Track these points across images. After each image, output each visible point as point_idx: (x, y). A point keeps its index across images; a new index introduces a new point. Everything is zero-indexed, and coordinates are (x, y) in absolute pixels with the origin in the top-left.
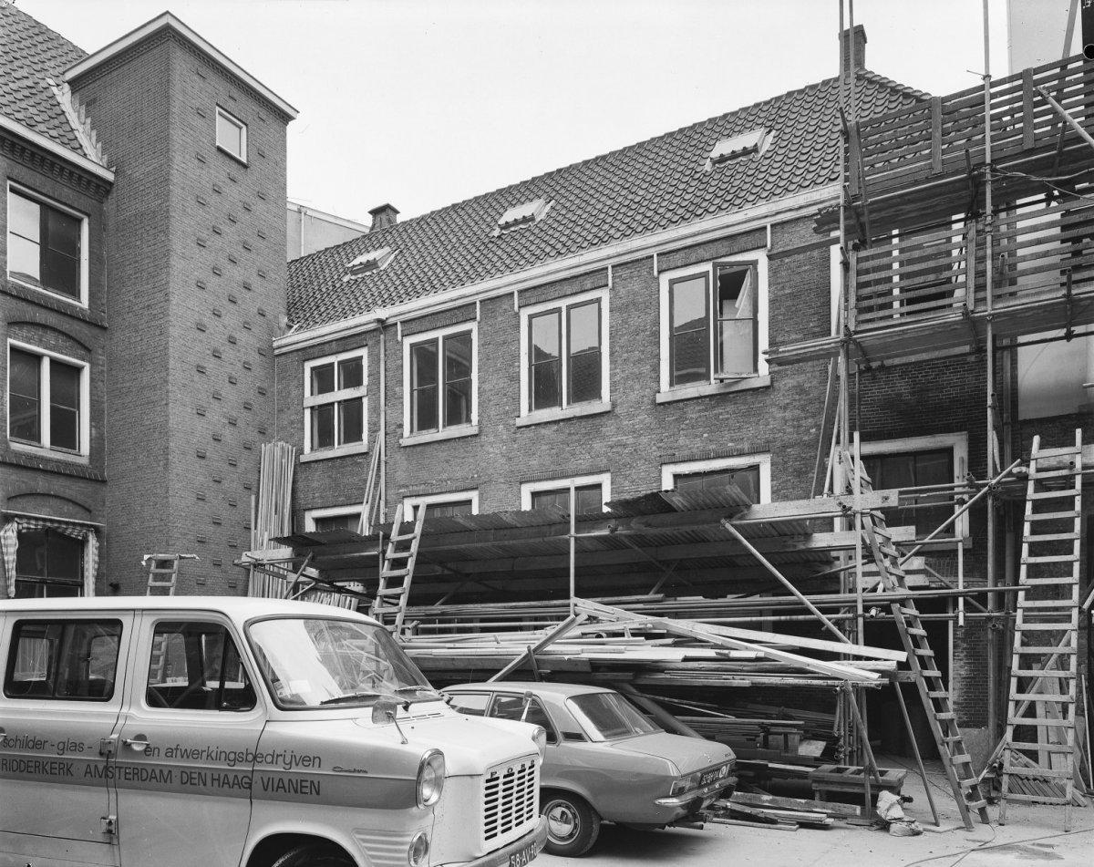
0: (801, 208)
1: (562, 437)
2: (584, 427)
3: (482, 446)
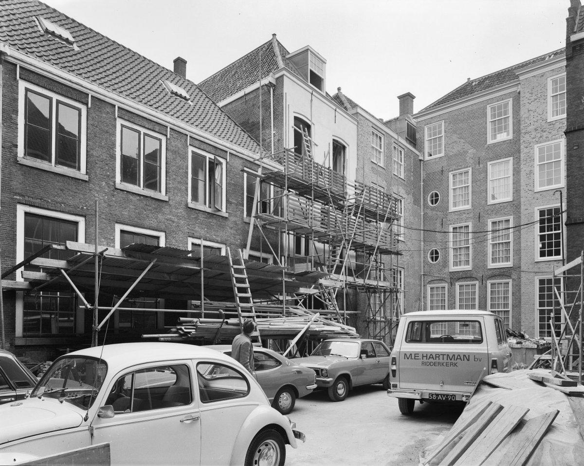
0: (238, 152)
1: (142, 205)
2: (154, 205)
3: (90, 190)
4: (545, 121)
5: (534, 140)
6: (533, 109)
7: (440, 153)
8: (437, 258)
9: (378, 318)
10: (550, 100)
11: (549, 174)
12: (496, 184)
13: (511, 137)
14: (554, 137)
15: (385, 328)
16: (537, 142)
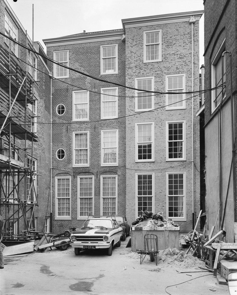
4: (142, 62)
5: (135, 74)
6: (134, 51)
7: (65, 75)
8: (63, 156)
9: (11, 201)
10: (145, 47)
11: (144, 101)
12: (107, 105)
13: (117, 72)
14: (148, 74)
15: (18, 211)
16: (137, 76)
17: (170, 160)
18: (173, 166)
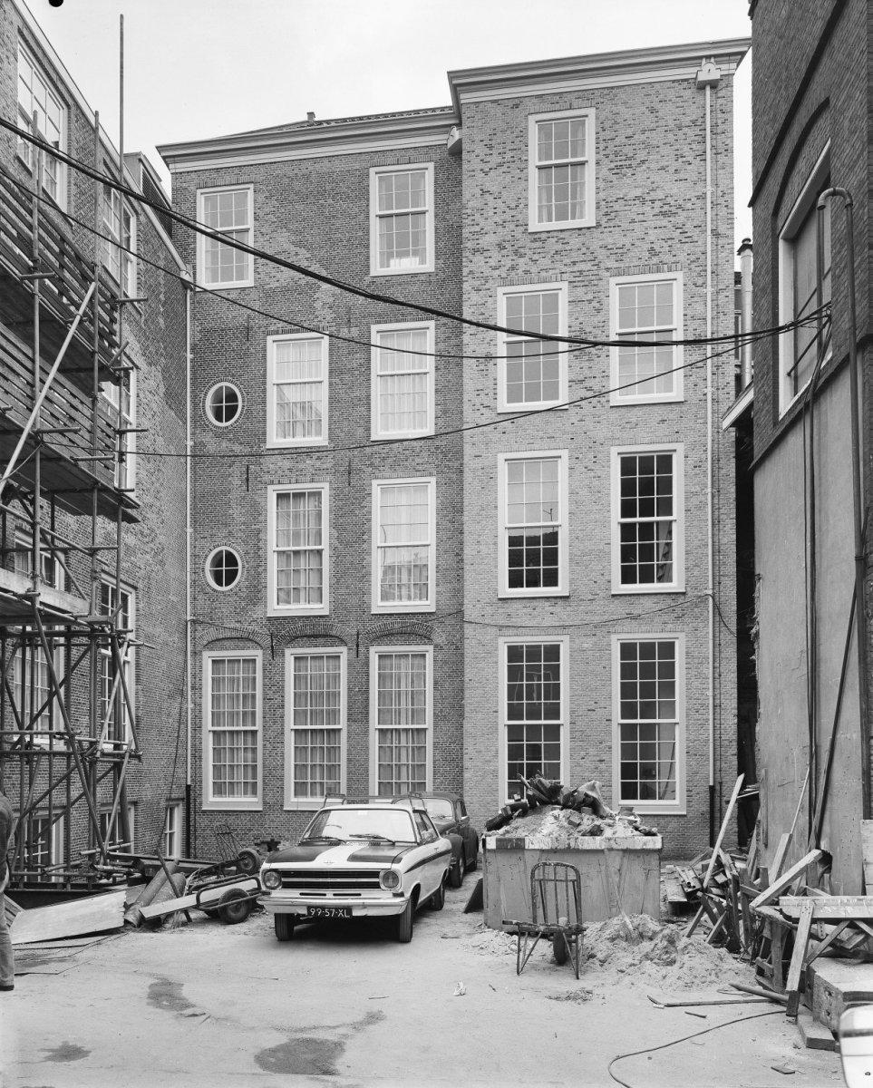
4: (522, 229)
5: (497, 272)
6: (494, 189)
7: (241, 277)
8: (231, 576)
9: (42, 741)
10: (533, 174)
11: (532, 373)
12: (393, 386)
13: (429, 266)
14: (543, 274)
15: (67, 777)
16: (505, 281)
17: (625, 590)
18: (636, 612)
